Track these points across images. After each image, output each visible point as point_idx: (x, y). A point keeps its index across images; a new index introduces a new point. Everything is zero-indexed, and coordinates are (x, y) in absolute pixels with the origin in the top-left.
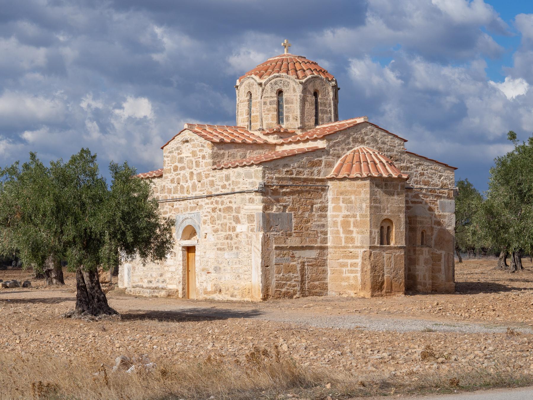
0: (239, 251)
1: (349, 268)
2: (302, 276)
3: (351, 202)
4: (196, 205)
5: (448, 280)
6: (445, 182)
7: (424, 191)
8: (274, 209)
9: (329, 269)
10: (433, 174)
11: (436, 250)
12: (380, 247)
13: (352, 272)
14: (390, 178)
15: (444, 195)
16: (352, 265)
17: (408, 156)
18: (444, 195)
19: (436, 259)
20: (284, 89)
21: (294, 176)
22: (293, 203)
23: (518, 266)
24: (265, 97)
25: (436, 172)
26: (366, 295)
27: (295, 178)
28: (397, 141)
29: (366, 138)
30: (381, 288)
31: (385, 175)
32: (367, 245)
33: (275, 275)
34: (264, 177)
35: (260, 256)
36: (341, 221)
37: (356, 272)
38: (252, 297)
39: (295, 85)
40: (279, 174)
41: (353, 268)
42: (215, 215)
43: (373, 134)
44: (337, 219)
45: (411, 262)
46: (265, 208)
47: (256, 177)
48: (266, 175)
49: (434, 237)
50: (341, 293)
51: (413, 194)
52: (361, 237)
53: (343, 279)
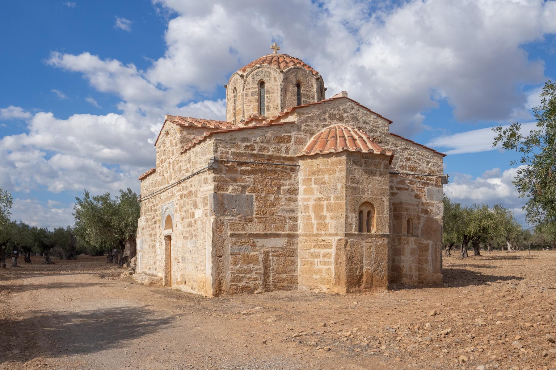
1: (322, 259)
2: (266, 268)
3: (324, 183)
6: (433, 168)
7: (410, 178)
8: (230, 190)
9: (299, 260)
10: (419, 160)
11: (423, 240)
12: (358, 235)
13: (324, 263)
14: (371, 153)
15: (431, 182)
16: (324, 256)
17: (393, 139)
19: (423, 249)
20: (265, 79)
21: (256, 152)
22: (254, 184)
23: (465, 255)
24: (247, 89)
25: (424, 158)
26: (340, 291)
28: (380, 122)
29: (345, 115)
30: (359, 282)
31: (364, 151)
32: (342, 231)
33: (230, 267)
34: (216, 151)
35: (211, 244)
36: (313, 205)
38: (206, 291)
39: (275, 75)
40: (237, 148)
41: (326, 260)
43: (353, 112)
44: (309, 203)
45: (395, 252)
46: (218, 188)
48: (219, 149)
49: (421, 226)
50: (312, 287)
51: (399, 180)
53: (314, 272)
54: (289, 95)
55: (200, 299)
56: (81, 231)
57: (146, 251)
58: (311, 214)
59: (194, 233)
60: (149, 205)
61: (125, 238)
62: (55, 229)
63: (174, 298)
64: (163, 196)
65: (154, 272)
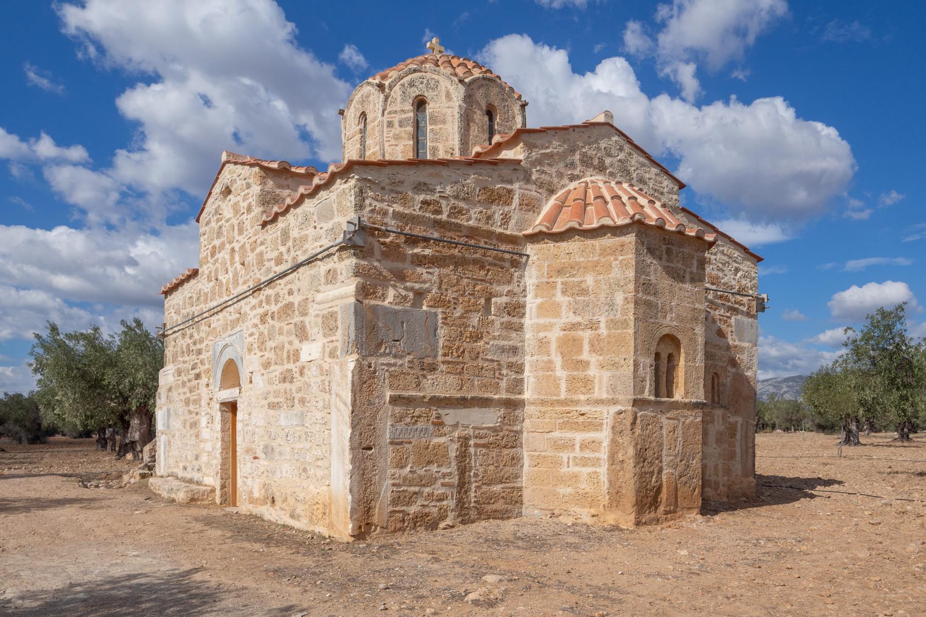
0: (306, 409)
1: (577, 453)
2: (463, 471)
3: (584, 292)
4: (238, 316)
5: (746, 475)
6: (743, 282)
8: (390, 297)
10: (724, 264)
13: (584, 462)
15: (741, 308)
16: (583, 446)
18: (741, 308)
20: (428, 95)
21: (444, 217)
22: (440, 288)
24: (390, 113)
25: (730, 261)
27: (448, 222)
29: (608, 161)
30: (655, 503)
34: (360, 206)
35: (348, 420)
36: (558, 339)
37: (596, 462)
38: (331, 526)
40: (404, 205)
41: (588, 454)
42: (264, 329)
43: (622, 156)
44: (549, 334)
46: (364, 292)
47: (342, 210)
48: (367, 202)
50: (556, 512)
52: (611, 378)
53: (561, 480)
54: (474, 130)
55: (318, 546)
56: (47, 394)
57: (177, 434)
58: (553, 357)
59: (297, 396)
60: (183, 343)
61: (130, 409)
62: (6, 394)
63: (257, 541)
64: (217, 321)
65: (196, 476)
